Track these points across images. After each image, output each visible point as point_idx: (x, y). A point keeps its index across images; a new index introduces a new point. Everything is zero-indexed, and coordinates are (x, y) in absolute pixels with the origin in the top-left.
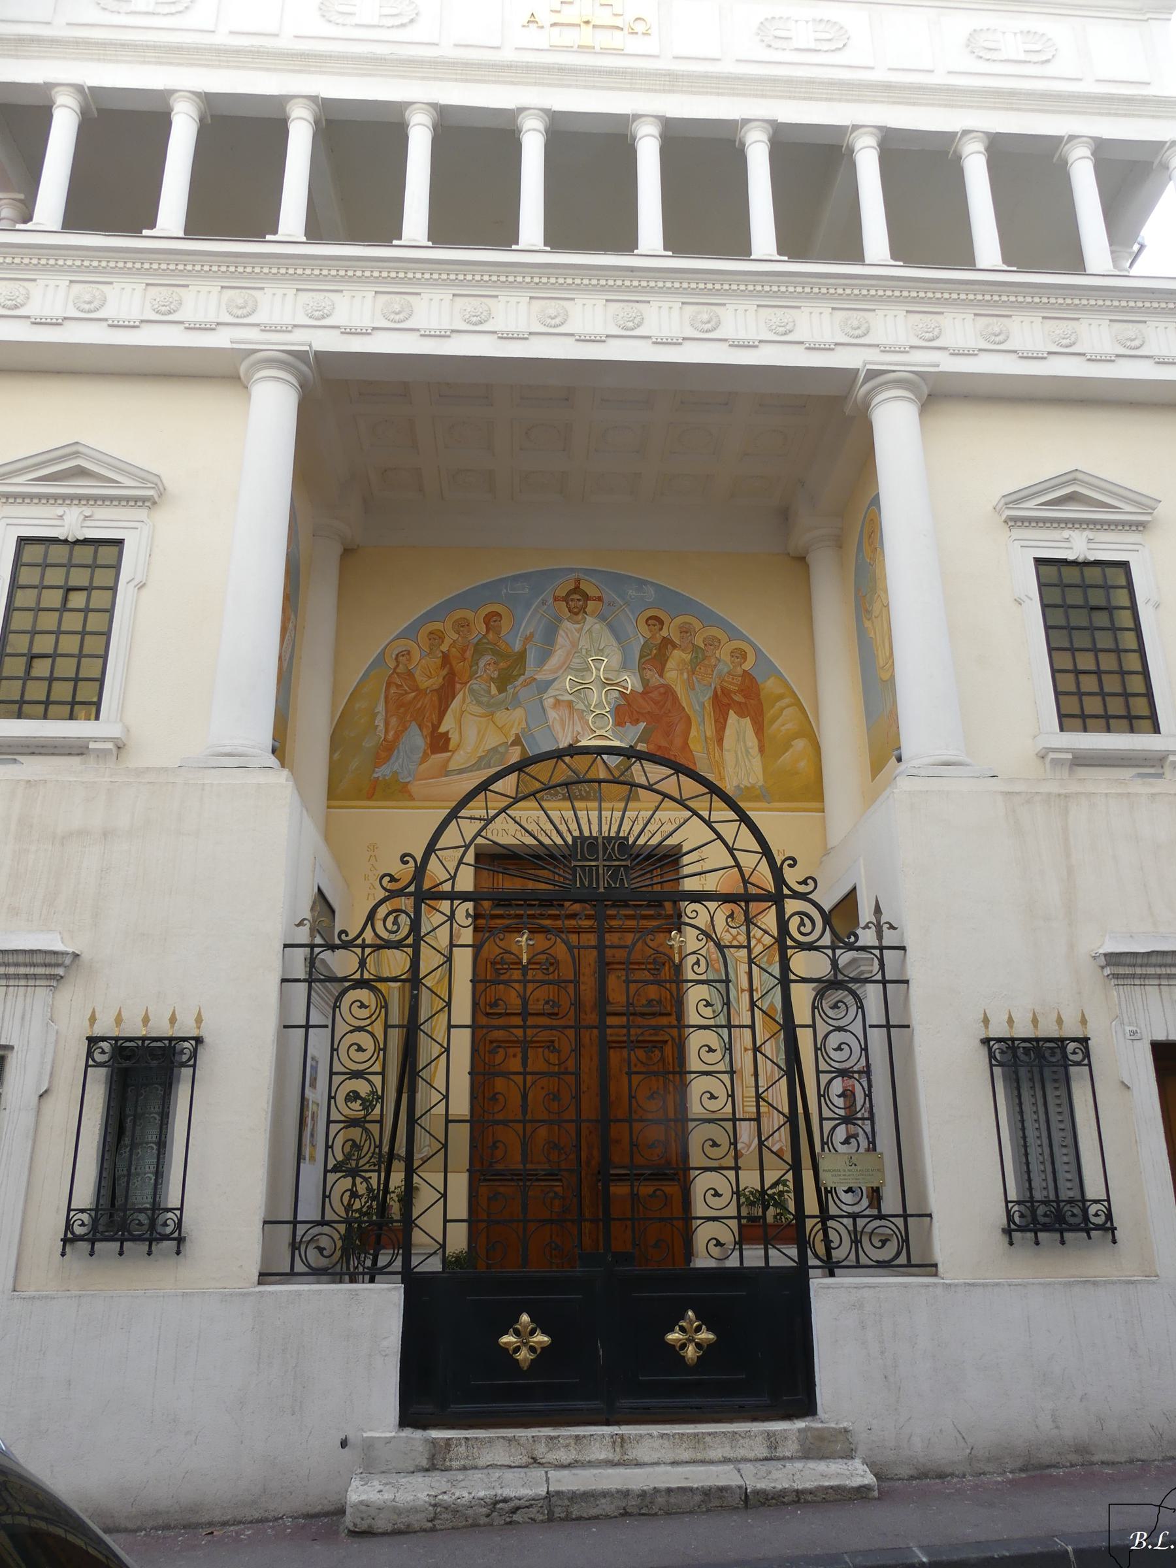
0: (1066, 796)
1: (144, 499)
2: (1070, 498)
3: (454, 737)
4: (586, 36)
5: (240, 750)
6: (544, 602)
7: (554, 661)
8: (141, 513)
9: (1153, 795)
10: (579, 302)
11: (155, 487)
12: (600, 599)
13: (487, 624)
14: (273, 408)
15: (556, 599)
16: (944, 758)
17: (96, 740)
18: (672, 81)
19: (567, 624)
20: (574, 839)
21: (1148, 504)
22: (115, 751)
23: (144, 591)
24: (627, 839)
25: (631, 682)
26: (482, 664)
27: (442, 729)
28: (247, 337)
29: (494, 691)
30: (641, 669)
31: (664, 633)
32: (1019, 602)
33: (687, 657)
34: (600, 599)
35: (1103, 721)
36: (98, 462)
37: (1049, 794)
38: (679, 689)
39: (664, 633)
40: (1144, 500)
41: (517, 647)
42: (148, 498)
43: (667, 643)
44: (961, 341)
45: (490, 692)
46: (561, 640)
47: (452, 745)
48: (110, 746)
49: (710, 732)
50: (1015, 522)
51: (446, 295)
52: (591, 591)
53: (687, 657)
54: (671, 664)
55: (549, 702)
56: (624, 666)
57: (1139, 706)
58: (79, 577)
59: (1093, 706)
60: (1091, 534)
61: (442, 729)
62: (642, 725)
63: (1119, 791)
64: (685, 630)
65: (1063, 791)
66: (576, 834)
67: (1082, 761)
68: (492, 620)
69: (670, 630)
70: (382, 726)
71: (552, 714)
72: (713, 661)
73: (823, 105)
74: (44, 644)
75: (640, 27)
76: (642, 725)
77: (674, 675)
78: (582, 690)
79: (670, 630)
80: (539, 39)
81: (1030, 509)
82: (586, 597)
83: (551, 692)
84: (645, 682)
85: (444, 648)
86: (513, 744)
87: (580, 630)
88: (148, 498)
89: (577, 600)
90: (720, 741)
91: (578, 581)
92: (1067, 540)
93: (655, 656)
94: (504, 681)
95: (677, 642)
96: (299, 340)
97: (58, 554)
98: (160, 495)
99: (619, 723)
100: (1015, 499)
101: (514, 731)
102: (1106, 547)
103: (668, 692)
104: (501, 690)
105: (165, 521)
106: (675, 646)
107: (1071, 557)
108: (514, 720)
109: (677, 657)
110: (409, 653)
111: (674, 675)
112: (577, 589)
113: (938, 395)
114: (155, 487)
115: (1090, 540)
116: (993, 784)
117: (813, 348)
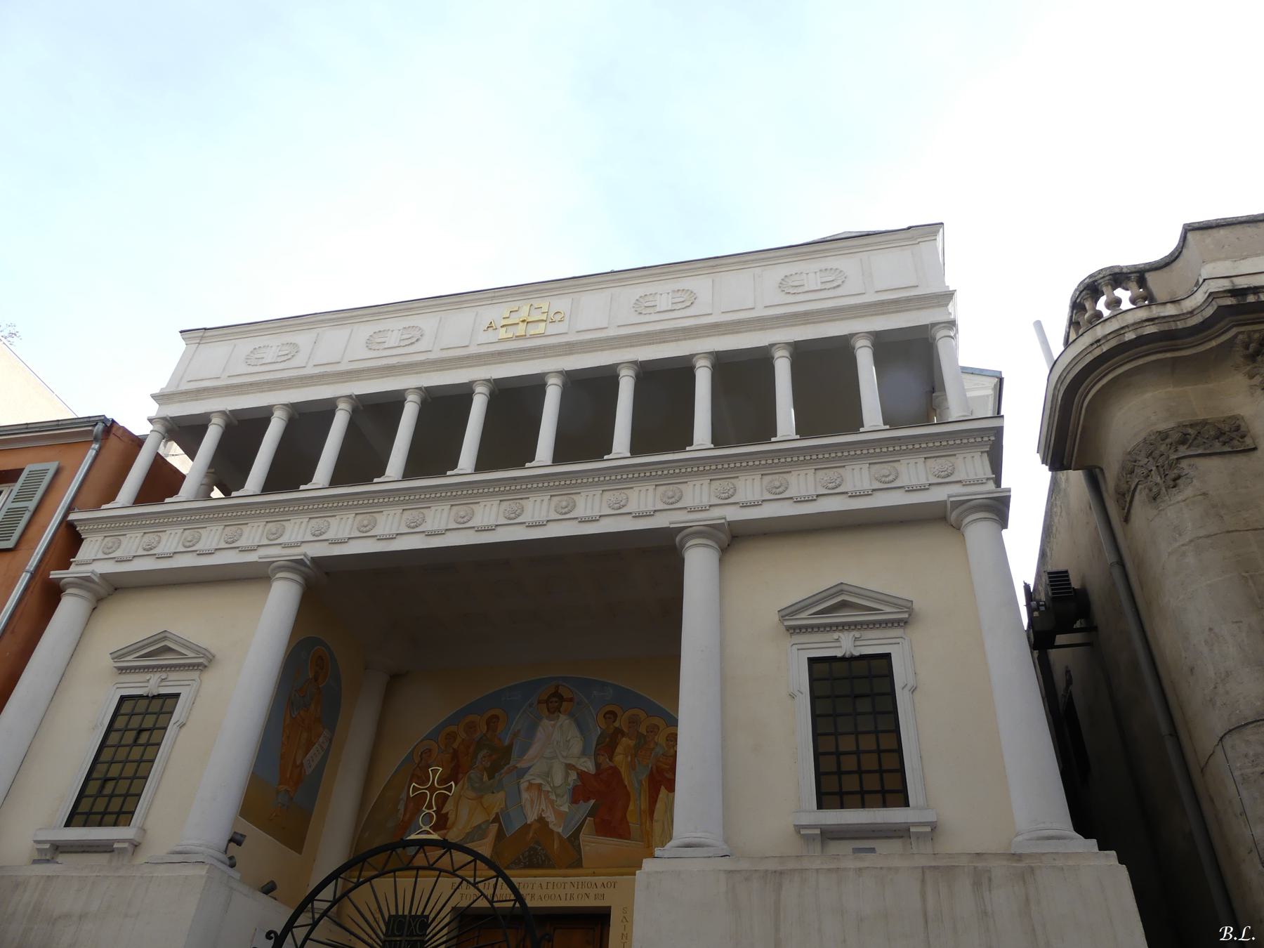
0: (781, 873)
1: (199, 665)
2: (838, 606)
3: (451, 817)
4: (521, 330)
5: (188, 848)
6: (530, 706)
7: (532, 752)
8: (194, 675)
9: (860, 869)
10: (482, 504)
11: (204, 656)
12: (571, 700)
13: (488, 724)
14: (281, 598)
15: (539, 702)
16: (687, 841)
17: (119, 841)
18: (570, 348)
19: (546, 722)
20: (390, 916)
21: (908, 607)
22: (131, 849)
23: (184, 729)
24: (427, 917)
25: (588, 766)
26: (480, 756)
27: (444, 811)
28: (274, 552)
29: (485, 778)
30: (596, 755)
31: (617, 724)
32: (792, 696)
33: (632, 743)
34: (571, 700)
35: (879, 796)
36: (176, 642)
37: (767, 871)
38: (623, 770)
39: (617, 724)
40: (900, 602)
41: (507, 743)
42: (201, 663)
43: (618, 732)
44: (752, 496)
45: (481, 779)
46: (540, 734)
47: (449, 823)
48: (126, 845)
49: (644, 805)
50: (794, 630)
51: (398, 510)
52: (566, 695)
53: (632, 743)
54: (619, 749)
55: (524, 785)
56: (584, 753)
57: (891, 782)
58: (149, 722)
59: (851, 783)
60: (857, 634)
61: (444, 811)
62: (592, 802)
63: (832, 866)
64: (634, 721)
65: (779, 868)
66: (393, 913)
67: (829, 835)
68: (492, 722)
69: (621, 723)
70: (402, 811)
71: (525, 795)
72: (652, 746)
73: (673, 345)
74: (115, 771)
75: (558, 317)
76: (592, 802)
77: (620, 759)
78: (548, 775)
79: (621, 723)
80: (491, 336)
81: (804, 619)
82: (561, 699)
83: (527, 777)
84: (598, 765)
85: (455, 746)
86: (493, 822)
87: (553, 726)
88: (201, 663)
89: (555, 702)
90: (652, 812)
91: (557, 687)
92: (837, 640)
93: (607, 745)
94: (493, 771)
95: (626, 730)
96: (296, 553)
97: (142, 705)
98: (210, 661)
99: (574, 801)
100: (788, 613)
101: (496, 810)
102: (871, 644)
103: (615, 772)
104: (491, 777)
105: (210, 681)
106: (623, 734)
107: (839, 655)
108: (496, 801)
109: (625, 742)
110: (430, 750)
111: (620, 759)
112: (556, 694)
113: (734, 539)
114: (204, 656)
115: (856, 639)
116: (726, 864)
117: (638, 516)
